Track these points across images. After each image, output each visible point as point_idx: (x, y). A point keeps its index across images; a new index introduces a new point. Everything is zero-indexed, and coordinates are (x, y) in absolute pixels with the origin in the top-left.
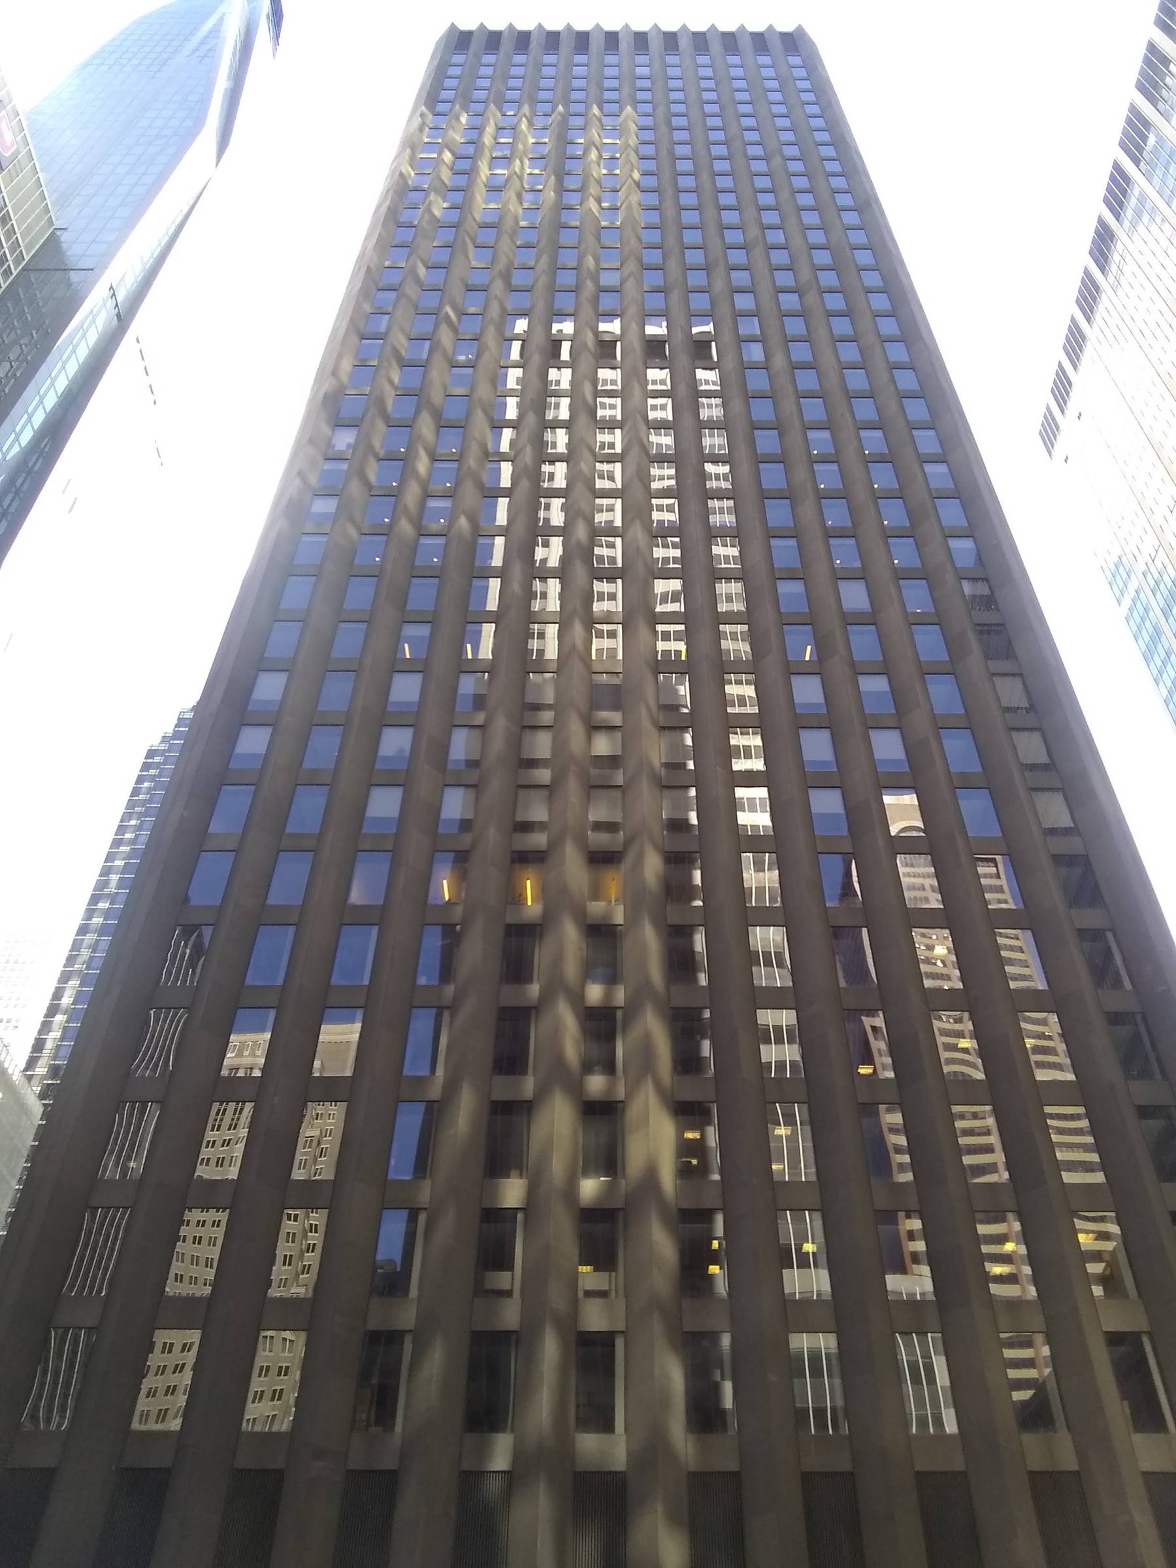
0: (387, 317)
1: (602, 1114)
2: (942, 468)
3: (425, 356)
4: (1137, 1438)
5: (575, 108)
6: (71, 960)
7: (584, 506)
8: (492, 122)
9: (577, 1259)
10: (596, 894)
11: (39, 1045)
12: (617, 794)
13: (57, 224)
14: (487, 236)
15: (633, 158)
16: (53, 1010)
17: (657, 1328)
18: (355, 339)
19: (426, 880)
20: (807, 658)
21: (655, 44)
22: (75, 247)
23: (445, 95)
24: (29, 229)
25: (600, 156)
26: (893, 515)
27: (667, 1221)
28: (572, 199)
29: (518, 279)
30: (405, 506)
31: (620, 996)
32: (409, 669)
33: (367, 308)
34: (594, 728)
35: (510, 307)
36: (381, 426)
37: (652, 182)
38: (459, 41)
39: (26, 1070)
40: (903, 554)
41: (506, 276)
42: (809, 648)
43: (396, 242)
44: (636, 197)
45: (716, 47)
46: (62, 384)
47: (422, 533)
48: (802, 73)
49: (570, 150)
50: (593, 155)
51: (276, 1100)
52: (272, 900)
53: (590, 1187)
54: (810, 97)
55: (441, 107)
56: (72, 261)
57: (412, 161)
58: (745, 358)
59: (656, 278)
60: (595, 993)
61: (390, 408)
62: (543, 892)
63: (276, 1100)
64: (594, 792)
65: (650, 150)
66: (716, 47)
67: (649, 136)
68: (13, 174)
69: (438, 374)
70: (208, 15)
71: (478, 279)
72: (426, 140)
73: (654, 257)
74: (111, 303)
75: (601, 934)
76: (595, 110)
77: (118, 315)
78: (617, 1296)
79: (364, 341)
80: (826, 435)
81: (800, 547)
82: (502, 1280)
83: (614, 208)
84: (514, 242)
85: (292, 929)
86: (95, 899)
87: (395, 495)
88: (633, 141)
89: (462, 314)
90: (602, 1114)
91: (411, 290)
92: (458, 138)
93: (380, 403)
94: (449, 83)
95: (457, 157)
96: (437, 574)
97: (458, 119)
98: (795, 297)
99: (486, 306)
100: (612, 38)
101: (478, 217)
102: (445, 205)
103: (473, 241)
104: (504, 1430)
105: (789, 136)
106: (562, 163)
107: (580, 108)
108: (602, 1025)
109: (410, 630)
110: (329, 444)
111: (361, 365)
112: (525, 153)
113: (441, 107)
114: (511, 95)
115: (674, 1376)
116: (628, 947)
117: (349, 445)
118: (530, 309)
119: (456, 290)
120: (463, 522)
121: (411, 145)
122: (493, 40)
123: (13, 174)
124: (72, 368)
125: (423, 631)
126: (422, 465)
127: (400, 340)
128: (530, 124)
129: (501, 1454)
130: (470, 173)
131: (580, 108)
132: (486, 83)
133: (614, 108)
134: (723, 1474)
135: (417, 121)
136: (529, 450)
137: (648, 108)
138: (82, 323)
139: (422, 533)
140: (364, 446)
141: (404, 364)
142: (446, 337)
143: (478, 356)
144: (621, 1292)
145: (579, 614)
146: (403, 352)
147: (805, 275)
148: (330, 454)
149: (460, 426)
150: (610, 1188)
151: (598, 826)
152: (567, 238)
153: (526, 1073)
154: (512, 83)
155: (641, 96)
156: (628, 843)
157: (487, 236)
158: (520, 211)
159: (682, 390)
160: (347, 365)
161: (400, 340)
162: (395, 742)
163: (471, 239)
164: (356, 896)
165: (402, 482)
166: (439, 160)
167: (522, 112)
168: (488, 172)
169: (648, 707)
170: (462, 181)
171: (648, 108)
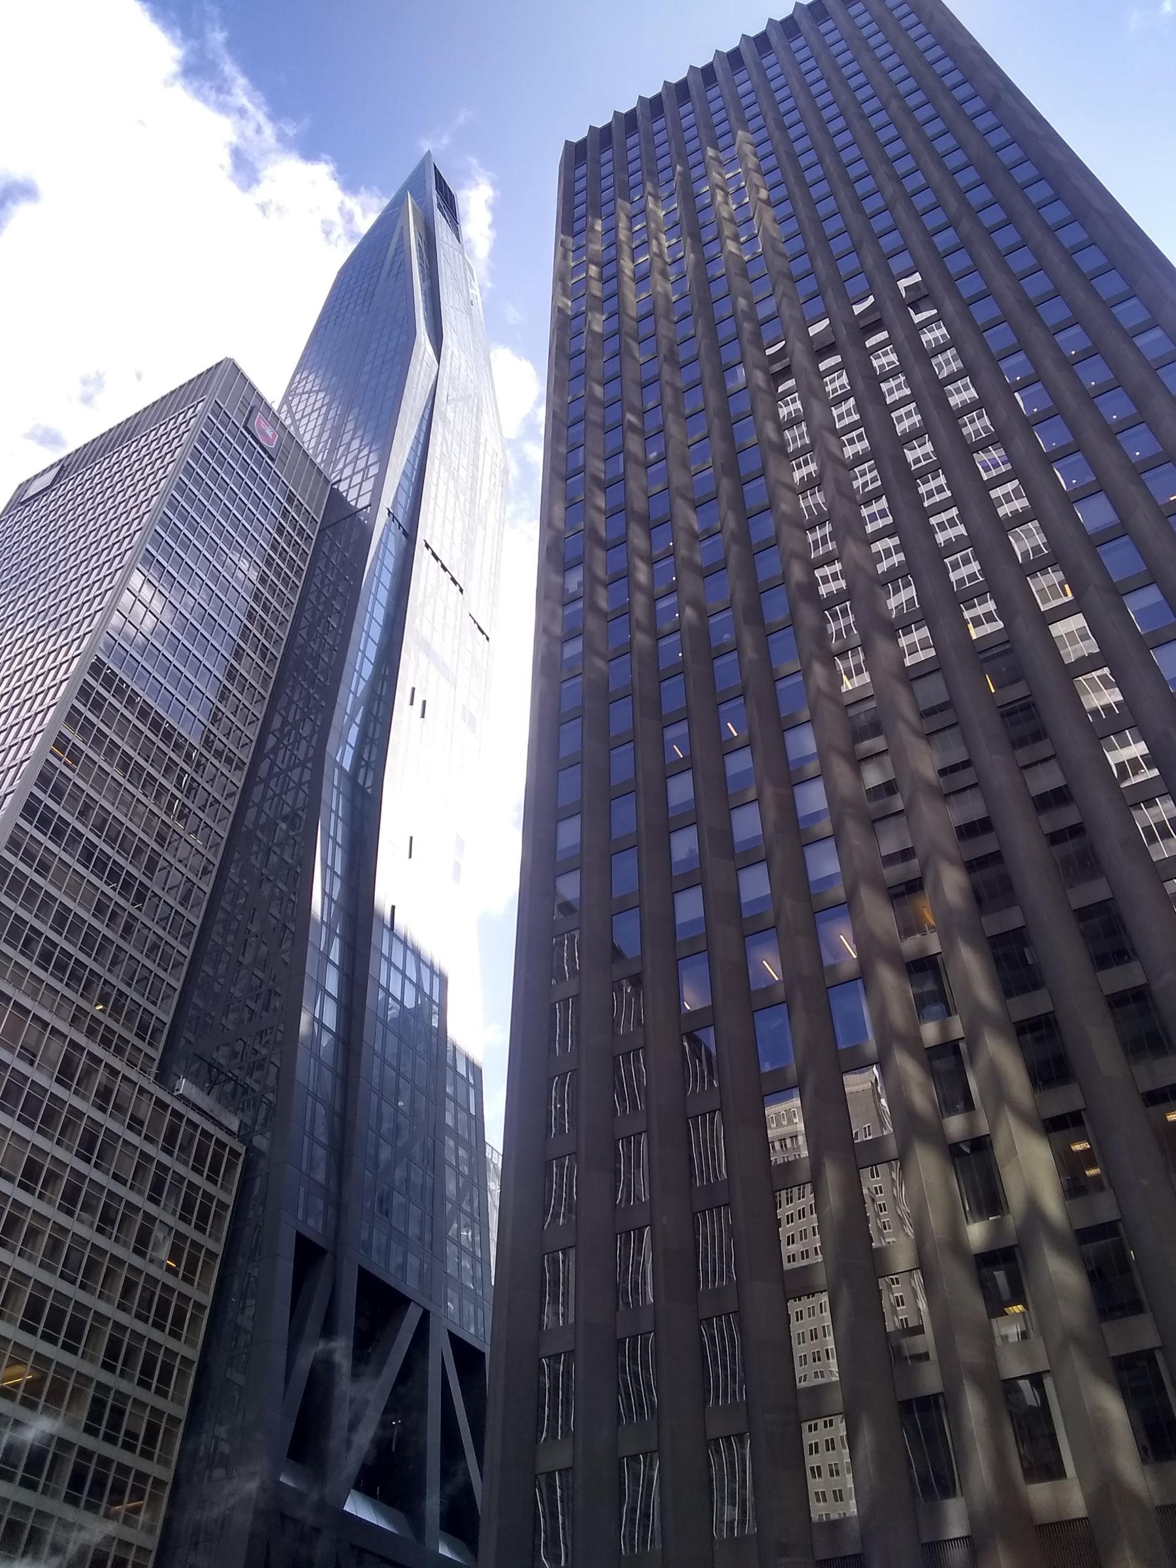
2: (1157, 334)
5: (692, 160)
10: (907, 930)
14: (647, 327)
15: (756, 178)
17: (1077, 1363)
18: (560, 485)
19: (742, 967)
23: (691, 147)
25: (727, 194)
26: (1115, 410)
27: (1061, 1247)
29: (684, 354)
30: (637, 620)
31: (957, 1029)
33: (563, 450)
34: (858, 762)
35: (681, 384)
36: (600, 554)
37: (781, 191)
41: (671, 358)
43: (572, 374)
44: (769, 214)
47: (658, 637)
50: (719, 197)
51: (664, 1220)
53: (976, 1233)
57: (565, 293)
59: (809, 285)
60: (930, 1032)
61: (603, 533)
64: (879, 827)
65: (771, 162)
67: (767, 148)
69: (636, 484)
71: (650, 372)
72: (573, 264)
73: (802, 265)
74: (394, 526)
75: (923, 968)
76: (710, 152)
77: (404, 532)
84: (670, 321)
87: (625, 611)
88: (752, 161)
89: (642, 414)
91: (595, 414)
92: (597, 247)
93: (592, 532)
95: (601, 266)
96: (679, 670)
97: (593, 229)
98: (950, 232)
101: (633, 313)
102: (604, 317)
103: (634, 339)
104: (955, 1495)
109: (671, 733)
110: (564, 590)
112: (659, 229)
113: (578, 226)
115: (1112, 1407)
116: (952, 976)
117: (579, 584)
118: (701, 377)
119: (633, 395)
120: (689, 612)
121: (561, 278)
125: (682, 729)
126: (642, 575)
127: (597, 466)
128: (656, 197)
129: (955, 1520)
130: (617, 275)
137: (759, 121)
138: (377, 553)
139: (658, 637)
140: (592, 579)
141: (605, 487)
142: (634, 444)
146: (603, 476)
149: (668, 520)
150: (998, 1228)
151: (889, 860)
152: (717, 290)
156: (923, 867)
157: (647, 327)
158: (669, 287)
159: (861, 385)
160: (559, 511)
161: (597, 466)
166: (588, 278)
168: (631, 266)
169: (907, 722)
171: (759, 121)
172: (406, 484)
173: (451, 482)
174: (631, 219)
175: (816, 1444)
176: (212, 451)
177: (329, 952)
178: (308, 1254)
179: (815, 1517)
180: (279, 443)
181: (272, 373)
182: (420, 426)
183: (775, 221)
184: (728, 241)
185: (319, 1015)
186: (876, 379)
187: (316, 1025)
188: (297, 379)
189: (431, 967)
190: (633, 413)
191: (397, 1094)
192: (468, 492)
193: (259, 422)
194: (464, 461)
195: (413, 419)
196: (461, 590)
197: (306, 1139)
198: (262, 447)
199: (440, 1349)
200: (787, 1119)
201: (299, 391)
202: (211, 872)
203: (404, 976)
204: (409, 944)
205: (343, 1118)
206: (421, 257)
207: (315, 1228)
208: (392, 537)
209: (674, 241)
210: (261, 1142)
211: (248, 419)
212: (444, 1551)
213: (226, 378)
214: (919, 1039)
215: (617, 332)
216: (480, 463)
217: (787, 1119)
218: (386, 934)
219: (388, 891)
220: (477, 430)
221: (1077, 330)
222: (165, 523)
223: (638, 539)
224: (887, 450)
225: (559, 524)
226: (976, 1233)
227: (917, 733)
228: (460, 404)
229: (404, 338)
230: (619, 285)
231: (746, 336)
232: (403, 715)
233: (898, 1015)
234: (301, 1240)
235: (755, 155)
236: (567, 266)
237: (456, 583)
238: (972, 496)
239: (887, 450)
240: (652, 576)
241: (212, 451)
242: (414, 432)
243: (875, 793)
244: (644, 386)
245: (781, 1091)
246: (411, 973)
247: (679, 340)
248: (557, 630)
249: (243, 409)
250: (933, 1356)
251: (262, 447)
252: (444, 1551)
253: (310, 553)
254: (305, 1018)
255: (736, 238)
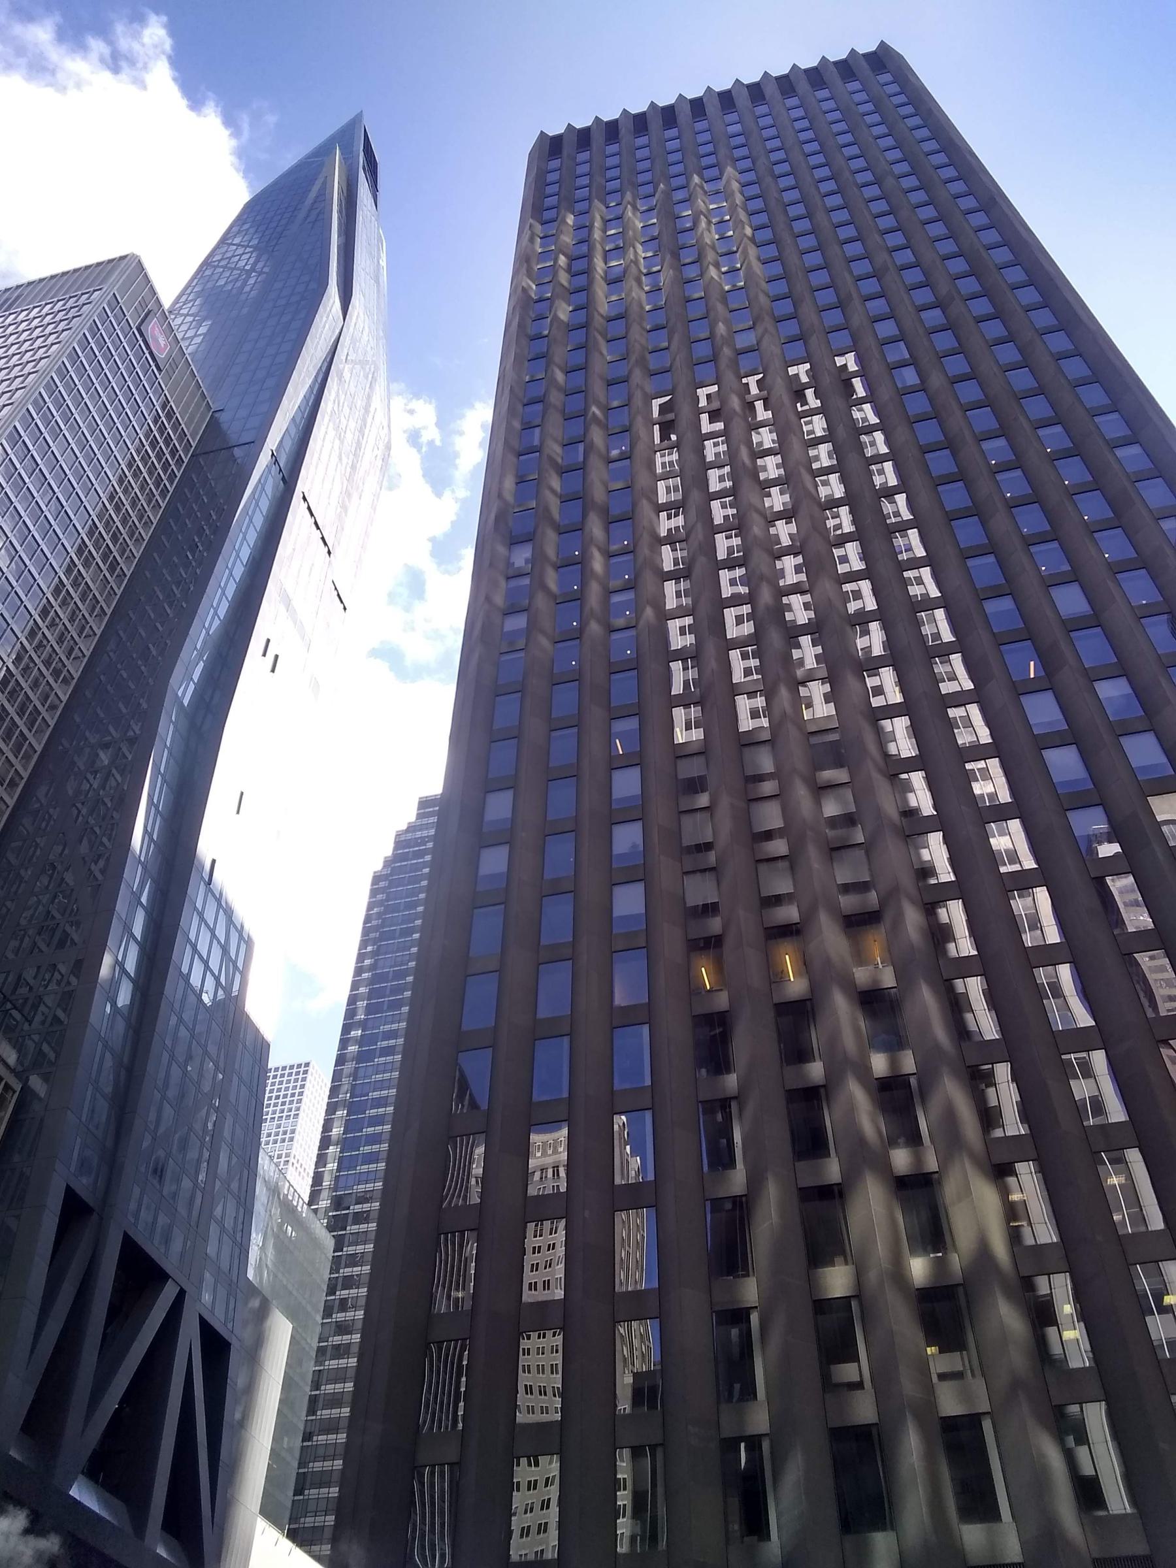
0: (537, 430)
1: (917, 1189)
2: (1135, 450)
3: (581, 459)
4: (261, 1524)
6: (334, 1091)
7: (765, 569)
8: (598, 217)
9: (923, 1342)
10: (860, 958)
11: (317, 1179)
12: (860, 854)
13: (214, 407)
14: (618, 328)
15: (743, 216)
16: (325, 1142)
18: (512, 459)
20: (1032, 676)
21: (743, 100)
22: (234, 427)
23: (550, 201)
24: (191, 419)
25: (709, 222)
28: (691, 272)
31: (909, 1063)
32: (626, 763)
33: (517, 425)
34: (821, 790)
37: (767, 234)
38: (550, 148)
39: (310, 1204)
40: (1113, 547)
42: (1032, 663)
44: (753, 251)
45: (803, 86)
46: (245, 553)
48: (895, 88)
49: (681, 224)
50: (703, 224)
52: (543, 1013)
53: (919, 1268)
54: (909, 109)
55: (548, 215)
56: (233, 439)
58: (900, 386)
59: (792, 328)
60: (879, 1064)
62: (805, 965)
63: (587, 1214)
64: (835, 854)
65: (758, 204)
66: (803, 86)
67: (754, 190)
68: (171, 372)
70: (312, 182)
73: (786, 307)
74: (275, 469)
75: (872, 1001)
76: (696, 179)
77: (283, 479)
78: (973, 1375)
79: (614, 560)
80: (1001, 442)
81: (1000, 563)
82: (848, 1372)
83: (733, 271)
85: (566, 1040)
86: (346, 1029)
87: (579, 598)
88: (739, 199)
89: (608, 410)
90: (917, 1189)
92: (567, 239)
94: (550, 190)
99: (630, 398)
100: (697, 106)
102: (571, 309)
103: (604, 336)
105: (896, 154)
106: (674, 242)
107: (681, 181)
108: (896, 1096)
109: (619, 726)
110: (509, 564)
111: (521, 481)
113: (548, 215)
114: (611, 185)
116: (910, 1014)
121: (524, 260)
122: (583, 137)
123: (171, 372)
124: (252, 537)
125: (632, 724)
126: (597, 564)
128: (635, 208)
130: (588, 272)
131: (681, 181)
132: (585, 181)
133: (714, 172)
134: (1133, 1559)
135: (527, 234)
136: (699, 526)
137: (747, 163)
138: (253, 493)
140: (538, 559)
141: (562, 472)
142: (597, 436)
143: (632, 447)
144: (978, 1372)
145: (780, 678)
146: (560, 461)
147: (944, 288)
148: (511, 573)
150: (940, 1266)
151: (846, 888)
152: (696, 311)
153: (829, 1155)
154: (611, 174)
155: (738, 153)
158: (643, 296)
160: (509, 483)
162: (627, 838)
163: (600, 334)
164: (620, 999)
165: (583, 585)
167: (624, 202)
170: (582, 280)
171: (747, 163)
172: (293, 432)
173: (337, 442)
174: (606, 223)
175: (536, 1481)
176: (102, 343)
177: (141, 894)
178: (75, 1209)
179: (514, 1556)
180: (169, 355)
181: (170, 281)
182: (318, 374)
183: (759, 259)
184: (711, 267)
185: (118, 960)
186: (781, 449)
187: (117, 969)
188: (183, 299)
189: (241, 931)
190: (599, 407)
191: (189, 1058)
192: (351, 457)
193: (153, 327)
194: (352, 425)
195: (311, 368)
196: (329, 553)
197: (90, 1088)
198: (151, 353)
199: (189, 1336)
200: (549, 1150)
201: (184, 311)
202: (17, 785)
203: (213, 935)
204: (223, 904)
205: (130, 1070)
206: (340, 212)
207: (84, 1186)
208: (270, 481)
209: (650, 254)
210: (36, 1082)
211: (143, 321)
212: (161, 1551)
213: (129, 269)
214: (868, 1068)
215: (585, 326)
216: (367, 431)
217: (549, 1150)
218: (202, 886)
219: (216, 840)
220: (369, 397)
221: (1058, 429)
222: (40, 403)
223: (595, 528)
224: (806, 508)
225: (509, 498)
226: (919, 1268)
227: (880, 771)
228: (358, 367)
229: (313, 285)
230: (591, 282)
231: (724, 362)
232: (253, 665)
233: (849, 1041)
234: (71, 1196)
235: (742, 193)
236: (533, 250)
237: (325, 544)
238: (885, 570)
239: (806, 508)
240: (607, 566)
241: (102, 343)
242: (309, 381)
243: (833, 822)
244: (610, 384)
245: (550, 1124)
246: (221, 933)
247: (650, 348)
248: (499, 600)
249: (140, 310)
250: (868, 1383)
251: (151, 353)
252: (161, 1551)
253: (179, 475)
254: (107, 960)
255: (717, 266)
